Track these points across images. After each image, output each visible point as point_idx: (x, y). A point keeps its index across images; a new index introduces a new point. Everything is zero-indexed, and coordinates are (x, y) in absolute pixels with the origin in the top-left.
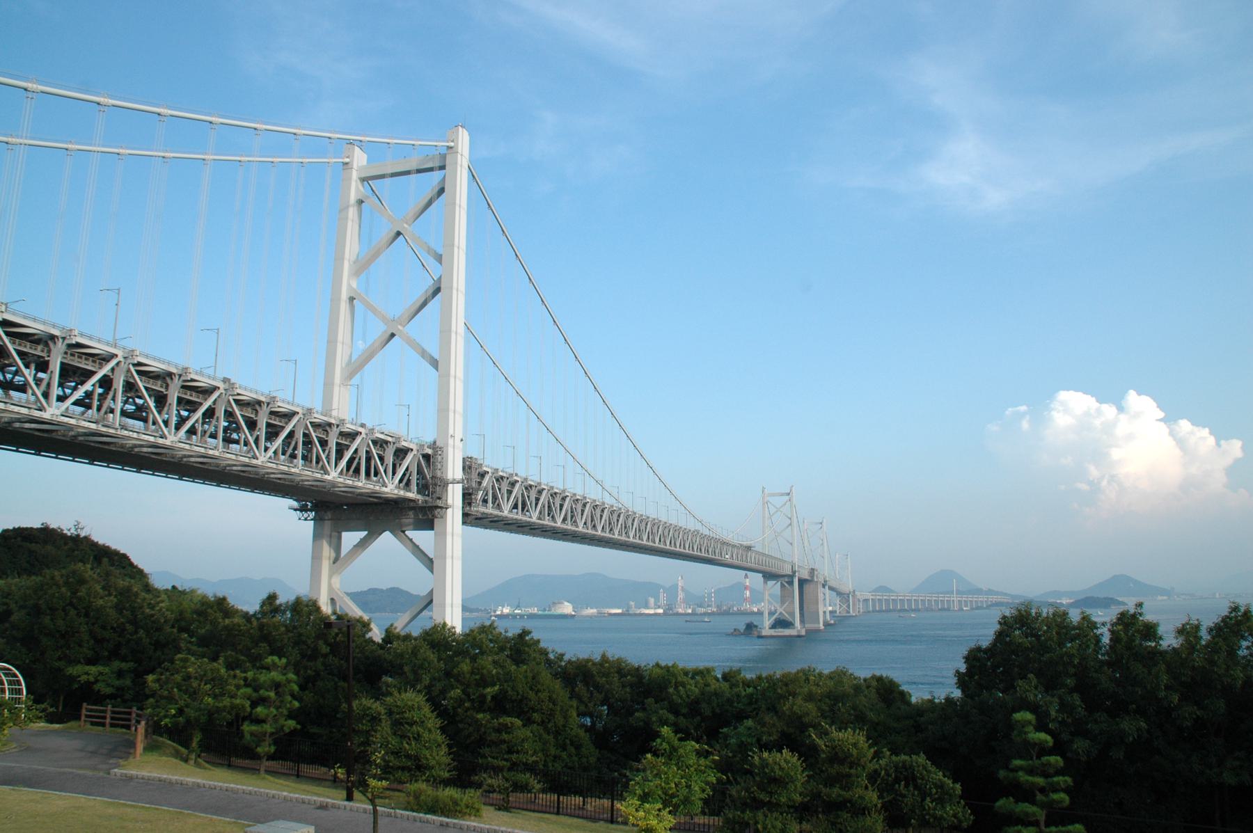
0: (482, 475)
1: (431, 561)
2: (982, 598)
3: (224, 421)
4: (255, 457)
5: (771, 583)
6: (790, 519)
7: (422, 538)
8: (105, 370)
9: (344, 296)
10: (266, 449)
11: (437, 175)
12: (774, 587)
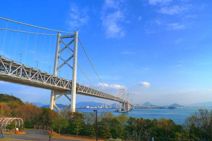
0: (79, 86)
2: (153, 107)
4: (28, 79)
5: (121, 103)
7: (68, 95)
8: (19, 68)
9: (57, 57)
10: (45, 81)
11: (73, 38)
12: (121, 104)
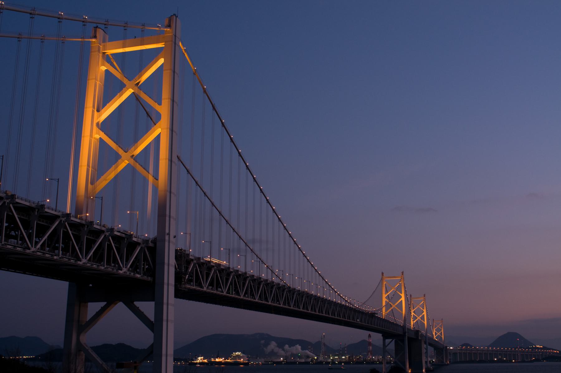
0: (189, 262)
3: (6, 223)
10: (37, 243)
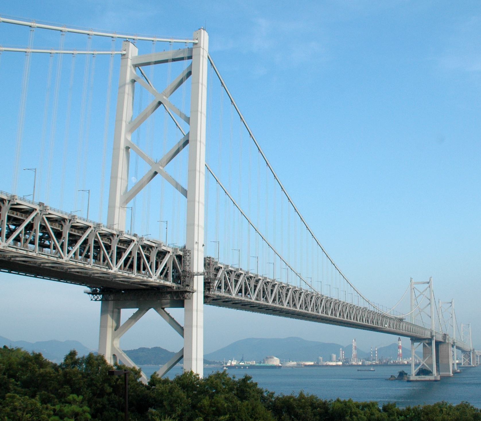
1: (182, 328)
4: (61, 257)
5: (416, 344)
6: (430, 300)
7: (176, 313)
9: (122, 146)
10: (69, 252)
11: (186, 63)
12: (419, 347)
